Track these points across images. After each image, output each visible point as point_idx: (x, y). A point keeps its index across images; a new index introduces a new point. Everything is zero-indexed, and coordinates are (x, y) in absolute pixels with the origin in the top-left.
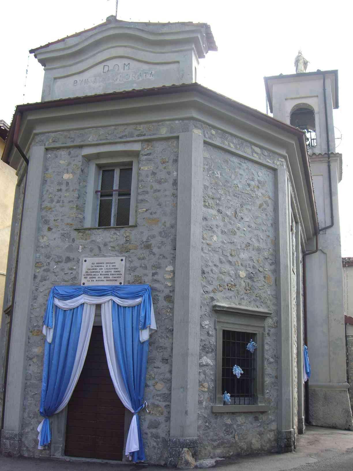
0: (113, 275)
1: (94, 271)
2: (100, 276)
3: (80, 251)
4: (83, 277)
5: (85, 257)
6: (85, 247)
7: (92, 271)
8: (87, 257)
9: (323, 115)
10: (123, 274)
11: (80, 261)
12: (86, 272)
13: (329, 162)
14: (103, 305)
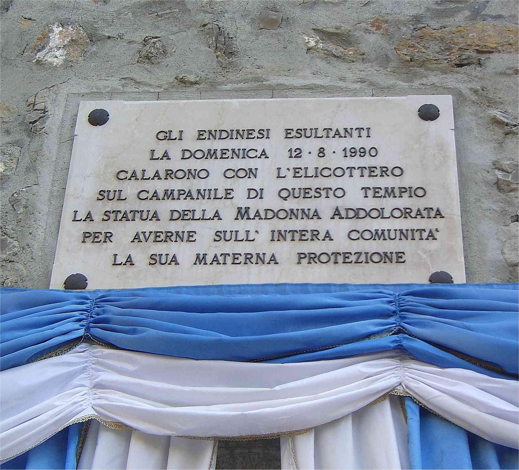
0: (357, 214)
1: (175, 185)
2: (228, 223)
3: (55, 56)
4: (71, 231)
5: (97, 94)
6: (94, 38)
7: (160, 186)
8: (112, 94)
10: (453, 209)
11: (53, 123)
12: (103, 195)
14: (306, 446)
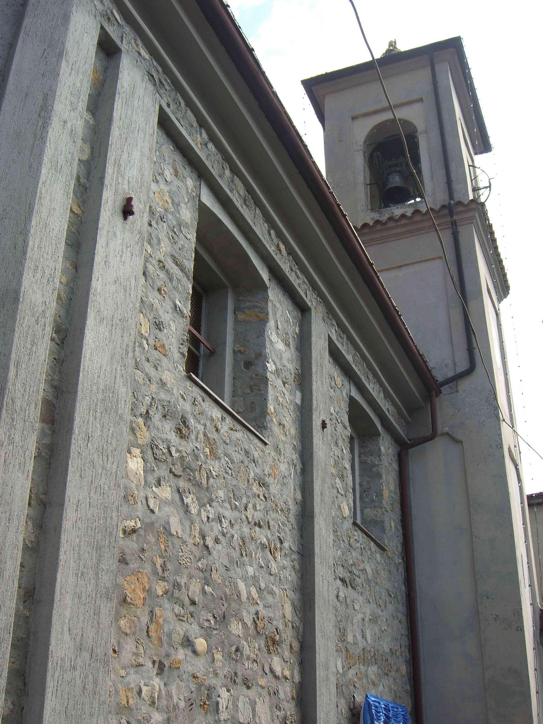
9: (435, 133)
13: (454, 224)
